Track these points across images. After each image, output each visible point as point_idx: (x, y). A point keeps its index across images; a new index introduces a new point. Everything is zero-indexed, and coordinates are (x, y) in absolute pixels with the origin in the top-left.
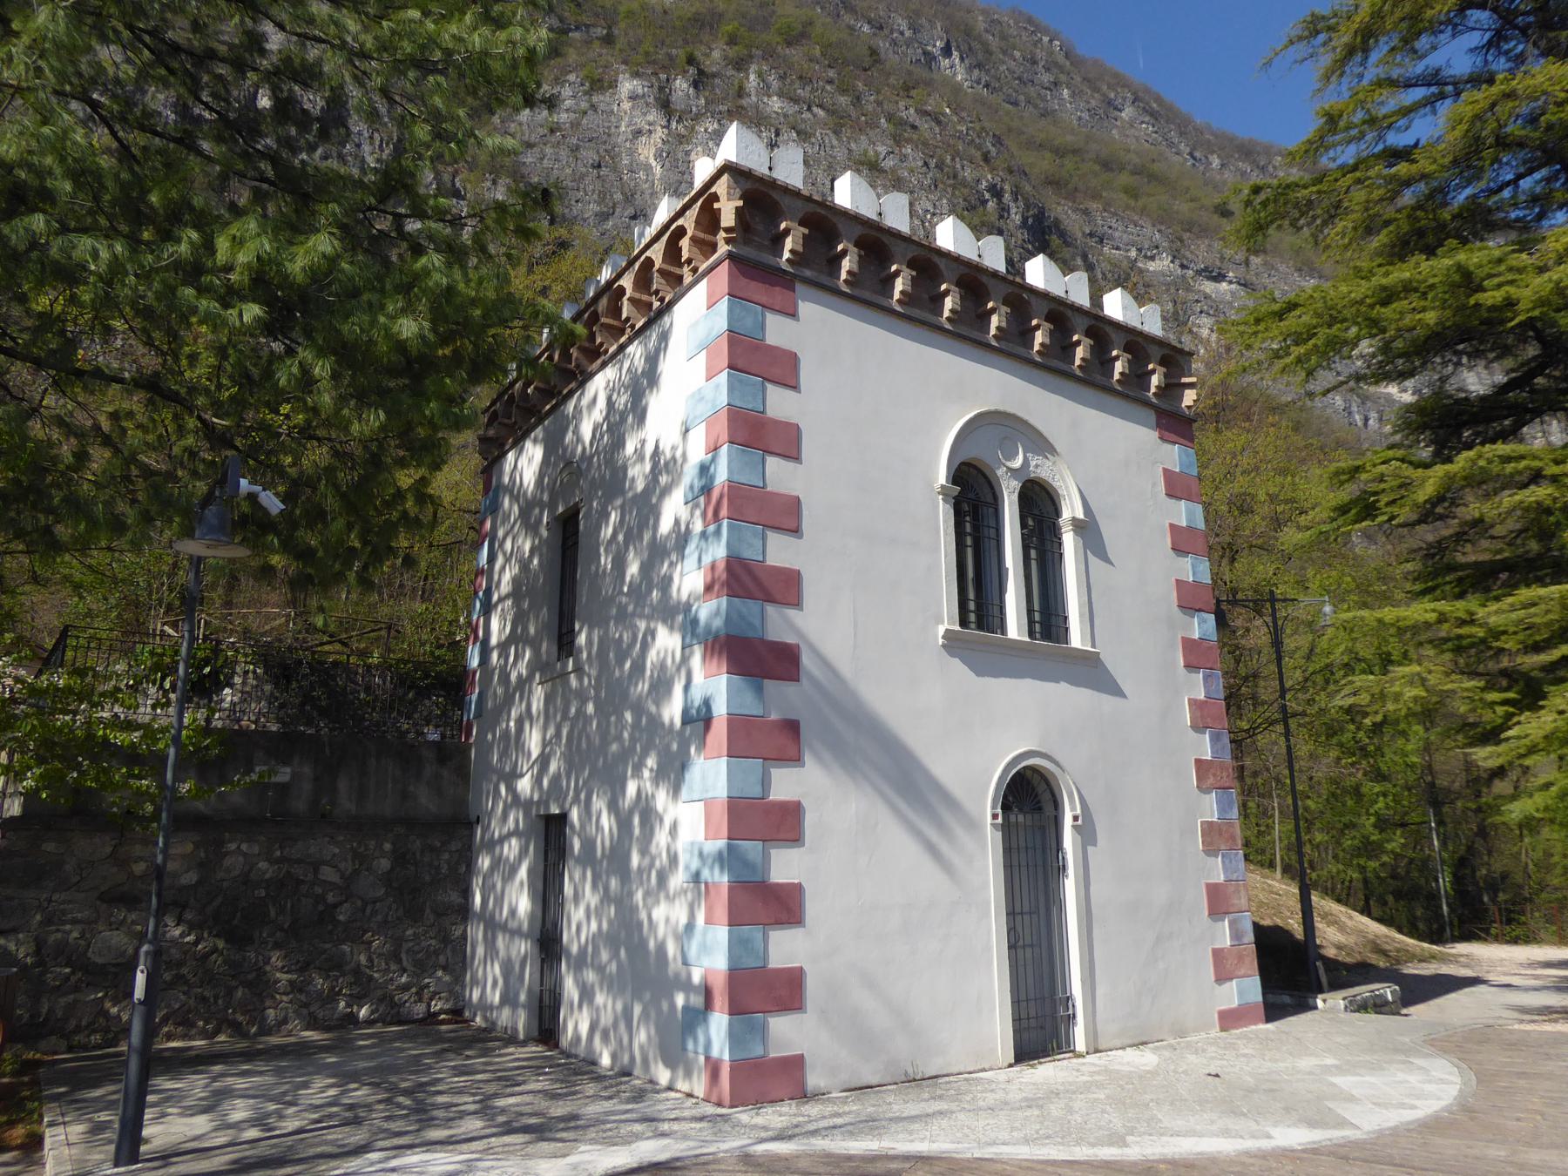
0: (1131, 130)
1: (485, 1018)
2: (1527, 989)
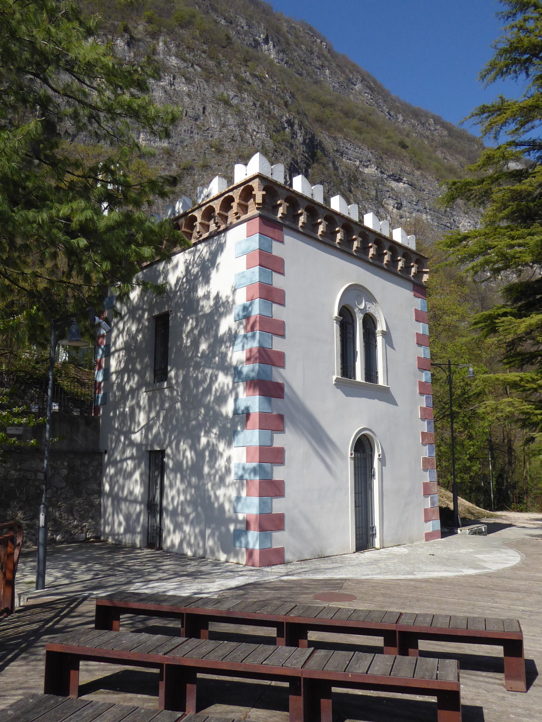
0: (359, 96)
1: (113, 539)
2: (531, 528)
